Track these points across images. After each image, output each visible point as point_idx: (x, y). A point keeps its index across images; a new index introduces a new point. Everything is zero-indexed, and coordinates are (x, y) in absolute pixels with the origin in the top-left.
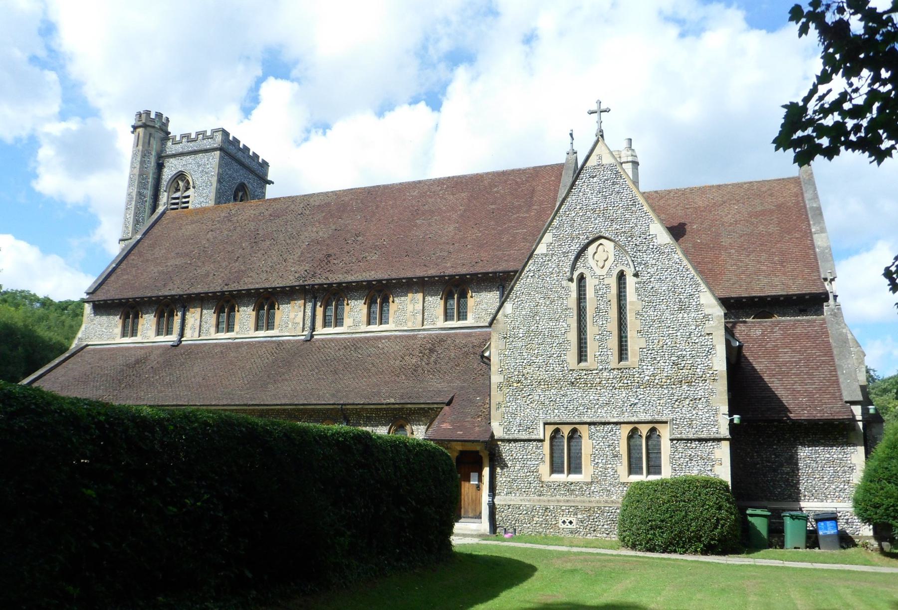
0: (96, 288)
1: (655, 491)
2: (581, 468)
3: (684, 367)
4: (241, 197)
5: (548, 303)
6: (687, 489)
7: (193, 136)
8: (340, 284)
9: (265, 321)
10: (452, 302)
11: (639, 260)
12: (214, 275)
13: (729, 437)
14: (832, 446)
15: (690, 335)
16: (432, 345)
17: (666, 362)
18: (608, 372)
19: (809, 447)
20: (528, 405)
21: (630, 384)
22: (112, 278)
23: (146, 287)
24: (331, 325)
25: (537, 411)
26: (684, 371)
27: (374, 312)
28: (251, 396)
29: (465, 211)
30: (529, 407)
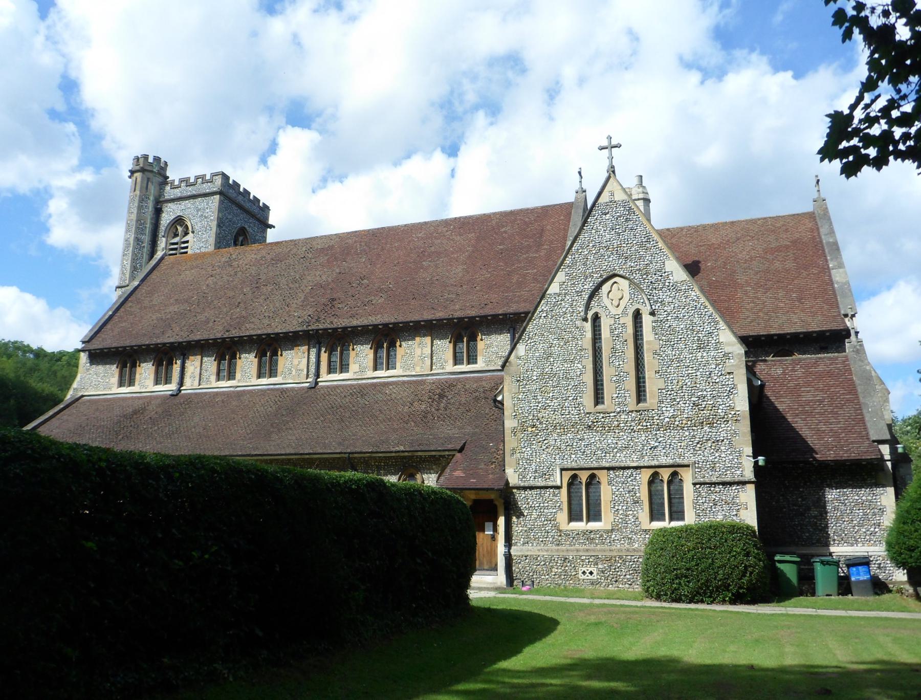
0: (91, 337)
1: (679, 537)
2: (600, 515)
3: (705, 407)
5: (562, 344)
7: (192, 180)
8: (345, 329)
9: (267, 368)
10: (461, 346)
13: (754, 479)
14: (861, 487)
15: (710, 374)
16: (442, 390)
17: (686, 403)
18: (626, 415)
19: (836, 489)
20: (543, 450)
21: (649, 427)
22: (108, 326)
25: (554, 456)
26: (705, 412)
27: (380, 357)
30: (545, 452)
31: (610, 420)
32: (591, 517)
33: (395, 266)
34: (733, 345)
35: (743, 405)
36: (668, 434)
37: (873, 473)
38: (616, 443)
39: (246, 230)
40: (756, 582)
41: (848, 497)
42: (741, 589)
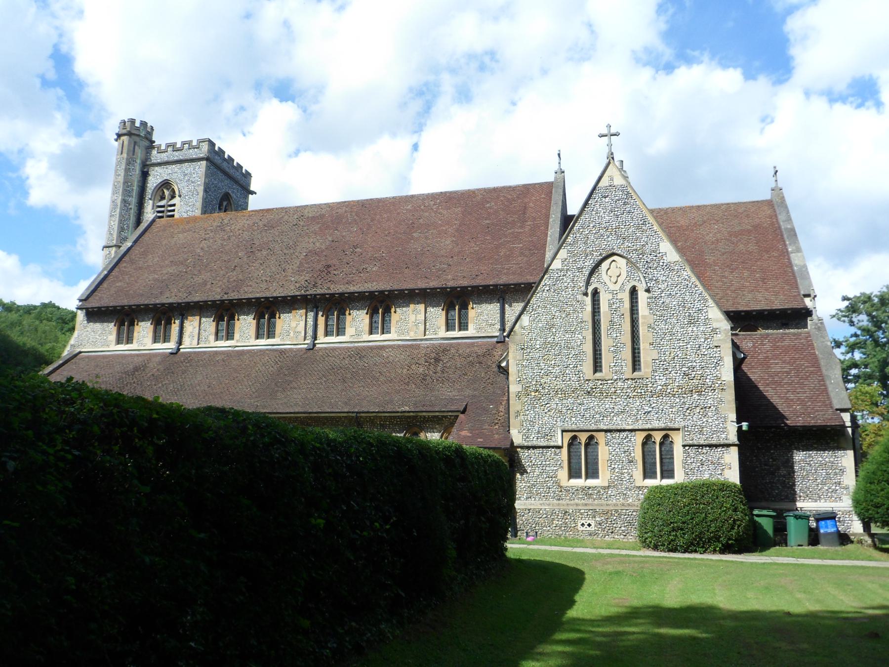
0: (88, 295)
1: (676, 494)
2: (598, 473)
3: (694, 377)
4: (226, 207)
5: (563, 316)
6: (706, 492)
7: (179, 145)
8: (342, 294)
9: (266, 330)
10: (453, 313)
11: (651, 276)
12: (212, 284)
13: (737, 442)
14: (824, 450)
15: (699, 347)
16: (437, 354)
17: (677, 373)
18: (623, 382)
19: (803, 451)
20: (546, 413)
21: (644, 393)
22: (105, 285)
23: (142, 295)
24: (333, 334)
25: (555, 419)
26: (694, 381)
27: (375, 322)
28: (262, 404)
29: (460, 226)
30: (547, 415)
31: (608, 387)
32: (589, 475)
33: (387, 236)
34: (721, 321)
35: (729, 376)
36: (661, 400)
37: (836, 438)
38: (613, 408)
39: (230, 195)
40: (743, 534)
41: (813, 458)
42: (730, 540)
